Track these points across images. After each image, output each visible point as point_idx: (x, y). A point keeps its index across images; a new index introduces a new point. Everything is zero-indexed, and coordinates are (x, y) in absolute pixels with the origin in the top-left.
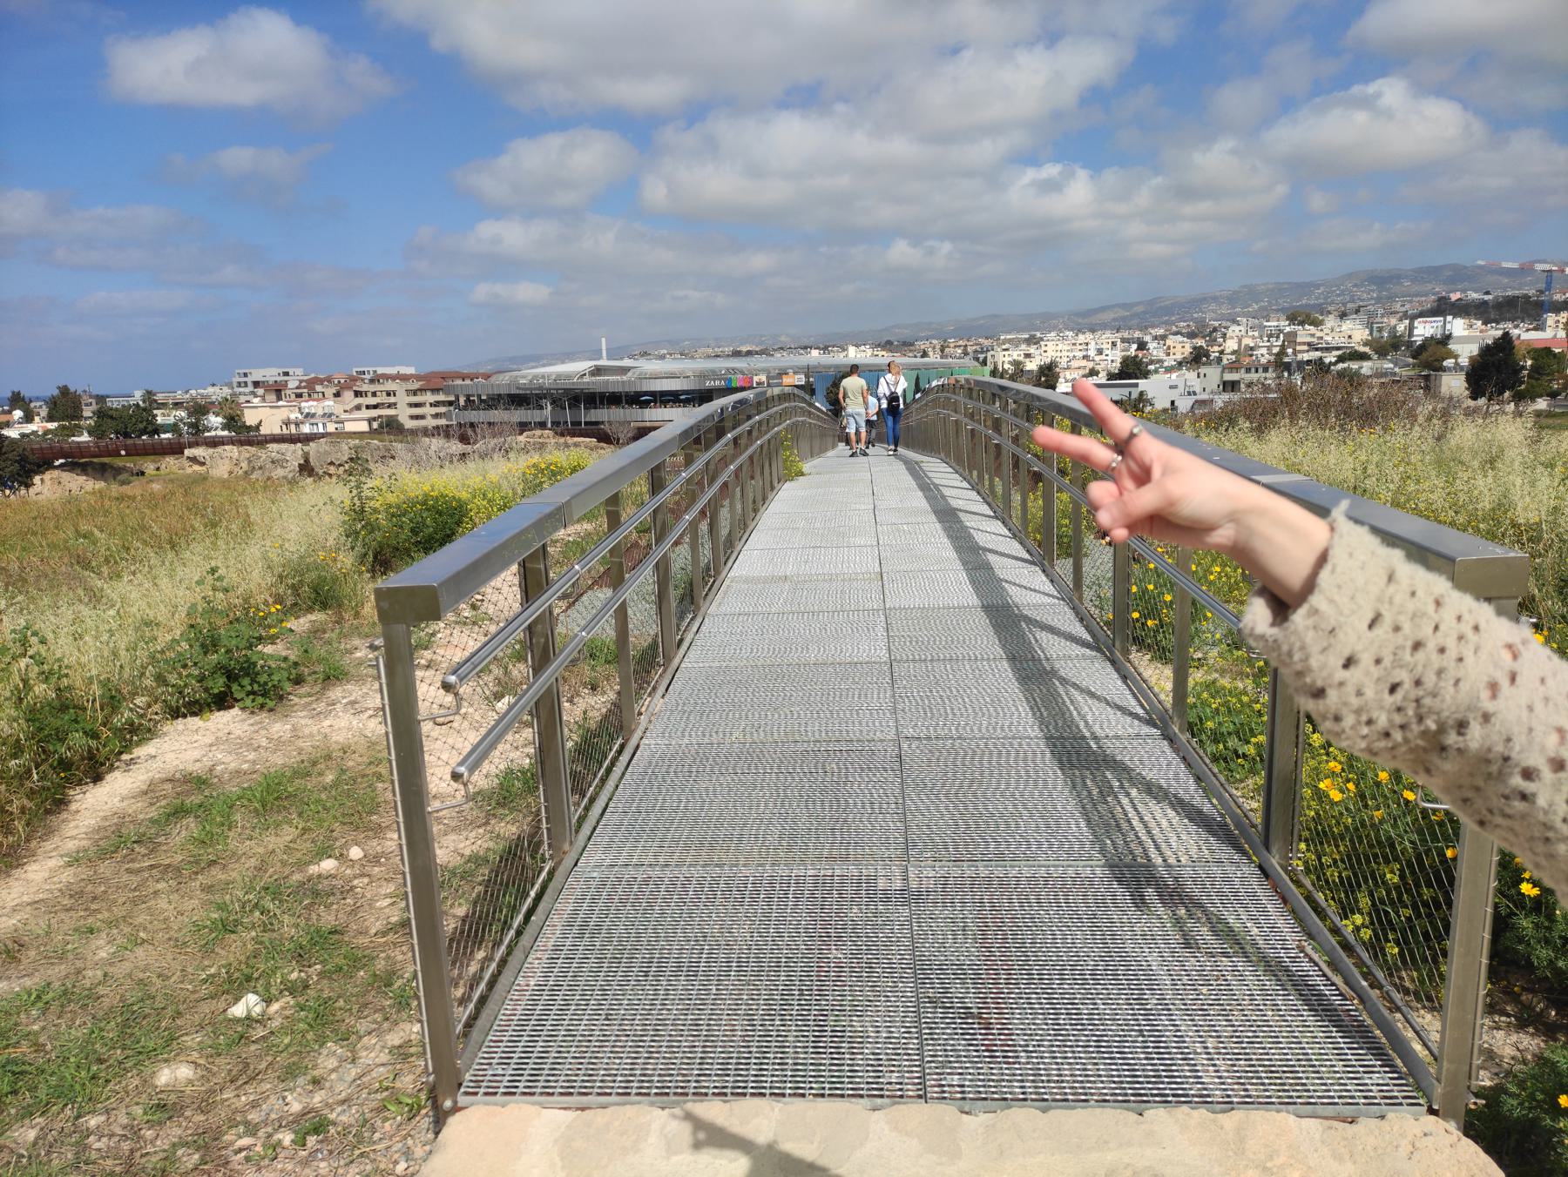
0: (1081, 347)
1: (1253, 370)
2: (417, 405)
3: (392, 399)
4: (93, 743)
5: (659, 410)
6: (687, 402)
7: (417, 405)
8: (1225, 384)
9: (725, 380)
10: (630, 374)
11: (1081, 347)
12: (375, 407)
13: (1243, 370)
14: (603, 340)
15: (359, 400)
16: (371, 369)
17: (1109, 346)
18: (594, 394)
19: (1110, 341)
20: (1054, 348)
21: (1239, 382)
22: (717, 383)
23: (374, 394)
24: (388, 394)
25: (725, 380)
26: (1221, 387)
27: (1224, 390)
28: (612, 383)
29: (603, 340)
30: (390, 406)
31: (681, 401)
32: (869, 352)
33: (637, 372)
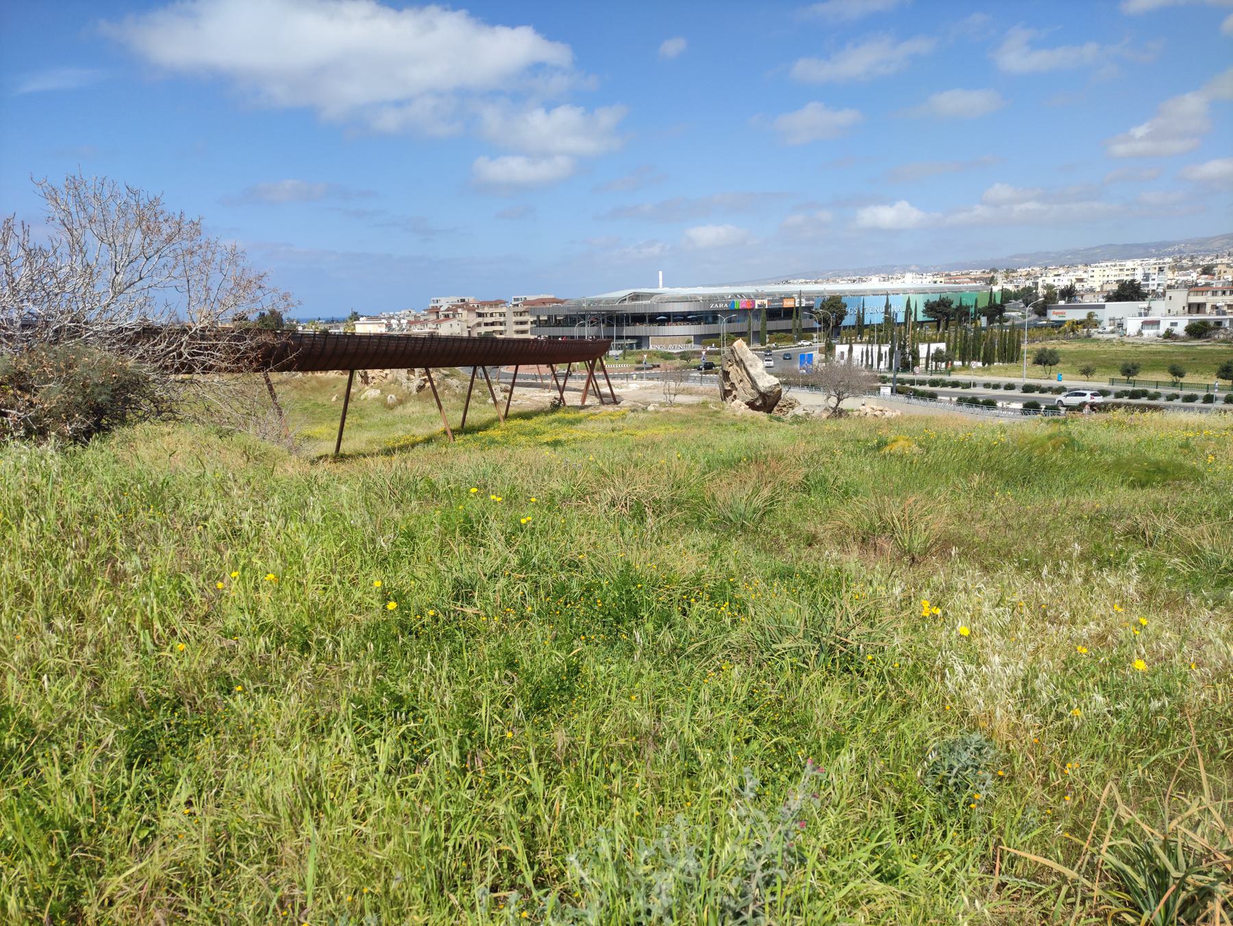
0: (1128, 273)
1: (1220, 293)
2: (522, 323)
3: (502, 319)
4: (806, 901)
5: (631, 328)
6: (692, 321)
7: (522, 323)
8: (1190, 305)
9: (728, 303)
10: (653, 299)
11: (1128, 273)
12: (492, 324)
13: (1209, 293)
14: (661, 273)
15: (480, 319)
16: (523, 297)
17: (1156, 271)
18: (622, 315)
19: (1157, 267)
20: (1101, 273)
21: (1204, 304)
22: (721, 306)
23: (492, 315)
24: (500, 315)
25: (728, 303)
26: (1187, 309)
27: (1189, 312)
28: (641, 306)
29: (661, 273)
30: (501, 324)
31: (657, 321)
32: (930, 279)
33: (658, 297)
